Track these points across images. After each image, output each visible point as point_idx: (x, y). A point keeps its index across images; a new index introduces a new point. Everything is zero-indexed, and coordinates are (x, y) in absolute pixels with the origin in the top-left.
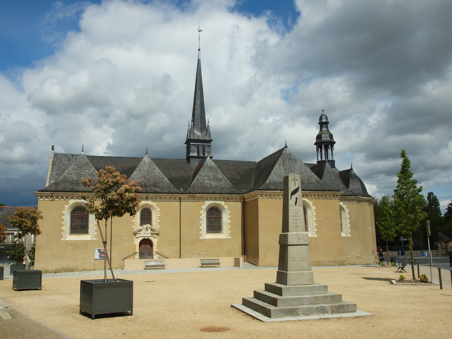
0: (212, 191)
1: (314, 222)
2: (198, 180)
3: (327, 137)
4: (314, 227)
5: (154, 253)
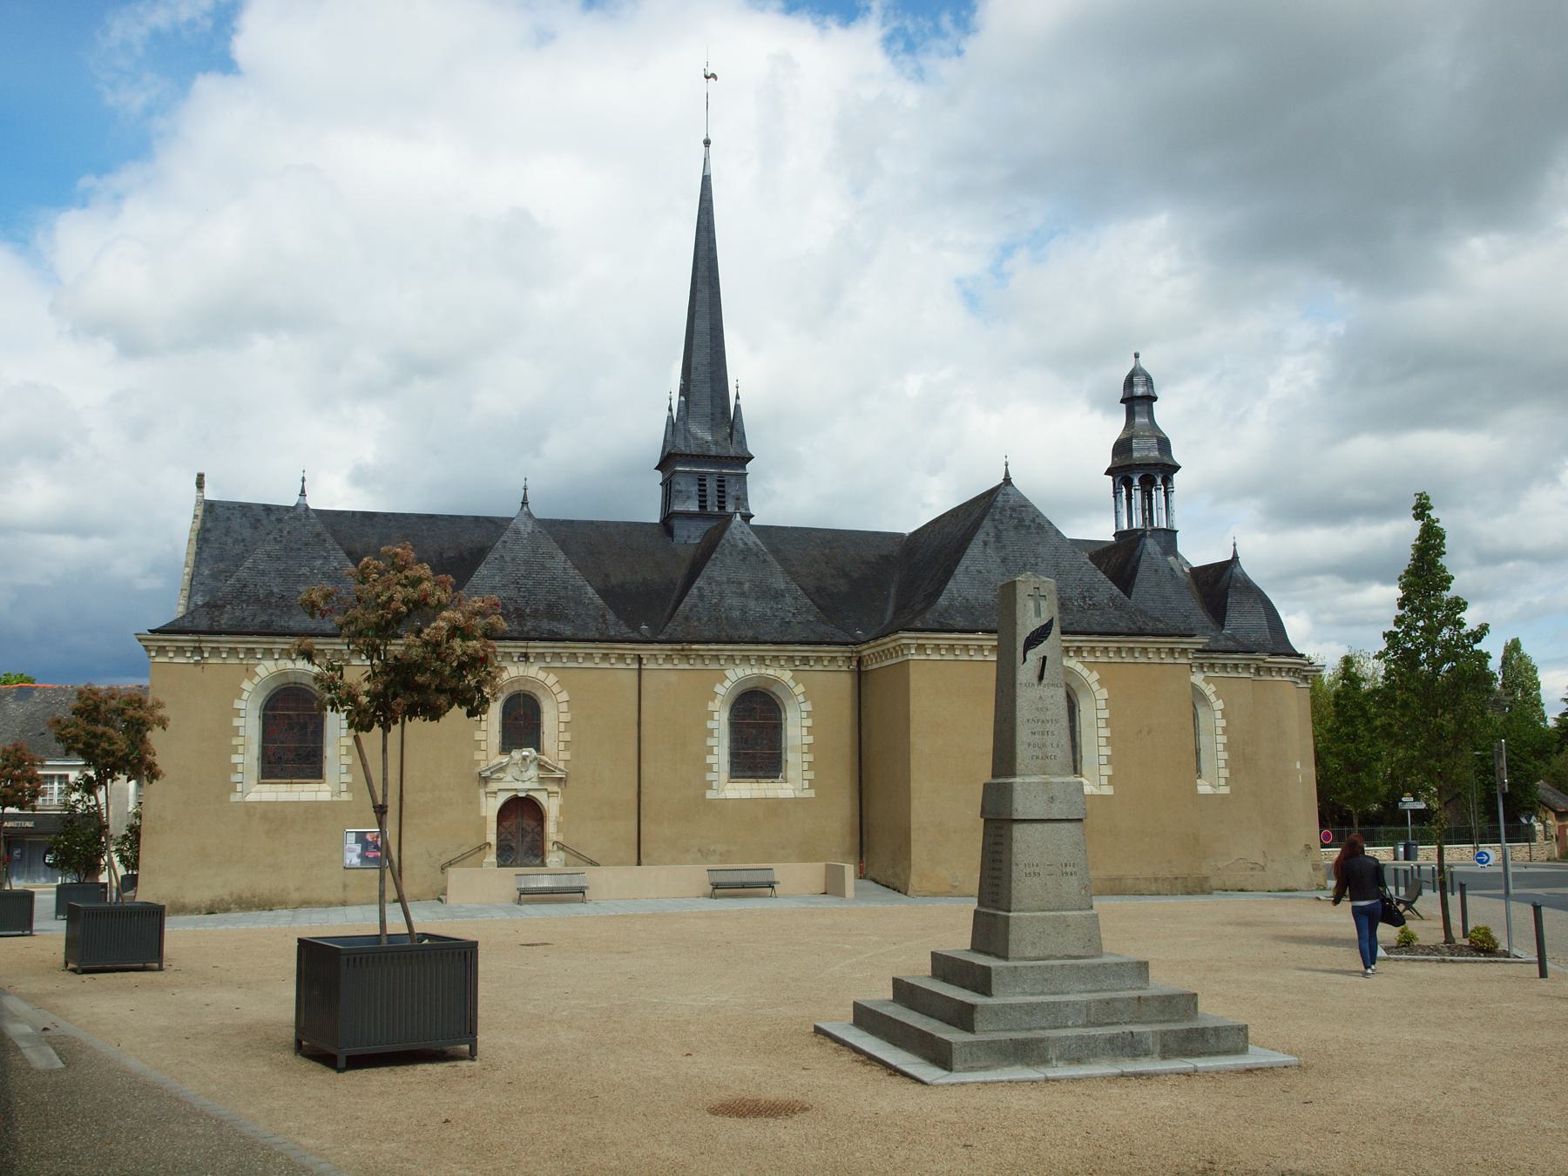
0: (750, 633)
1: (1103, 742)
2: (701, 597)
4: (1104, 760)
5: (549, 846)
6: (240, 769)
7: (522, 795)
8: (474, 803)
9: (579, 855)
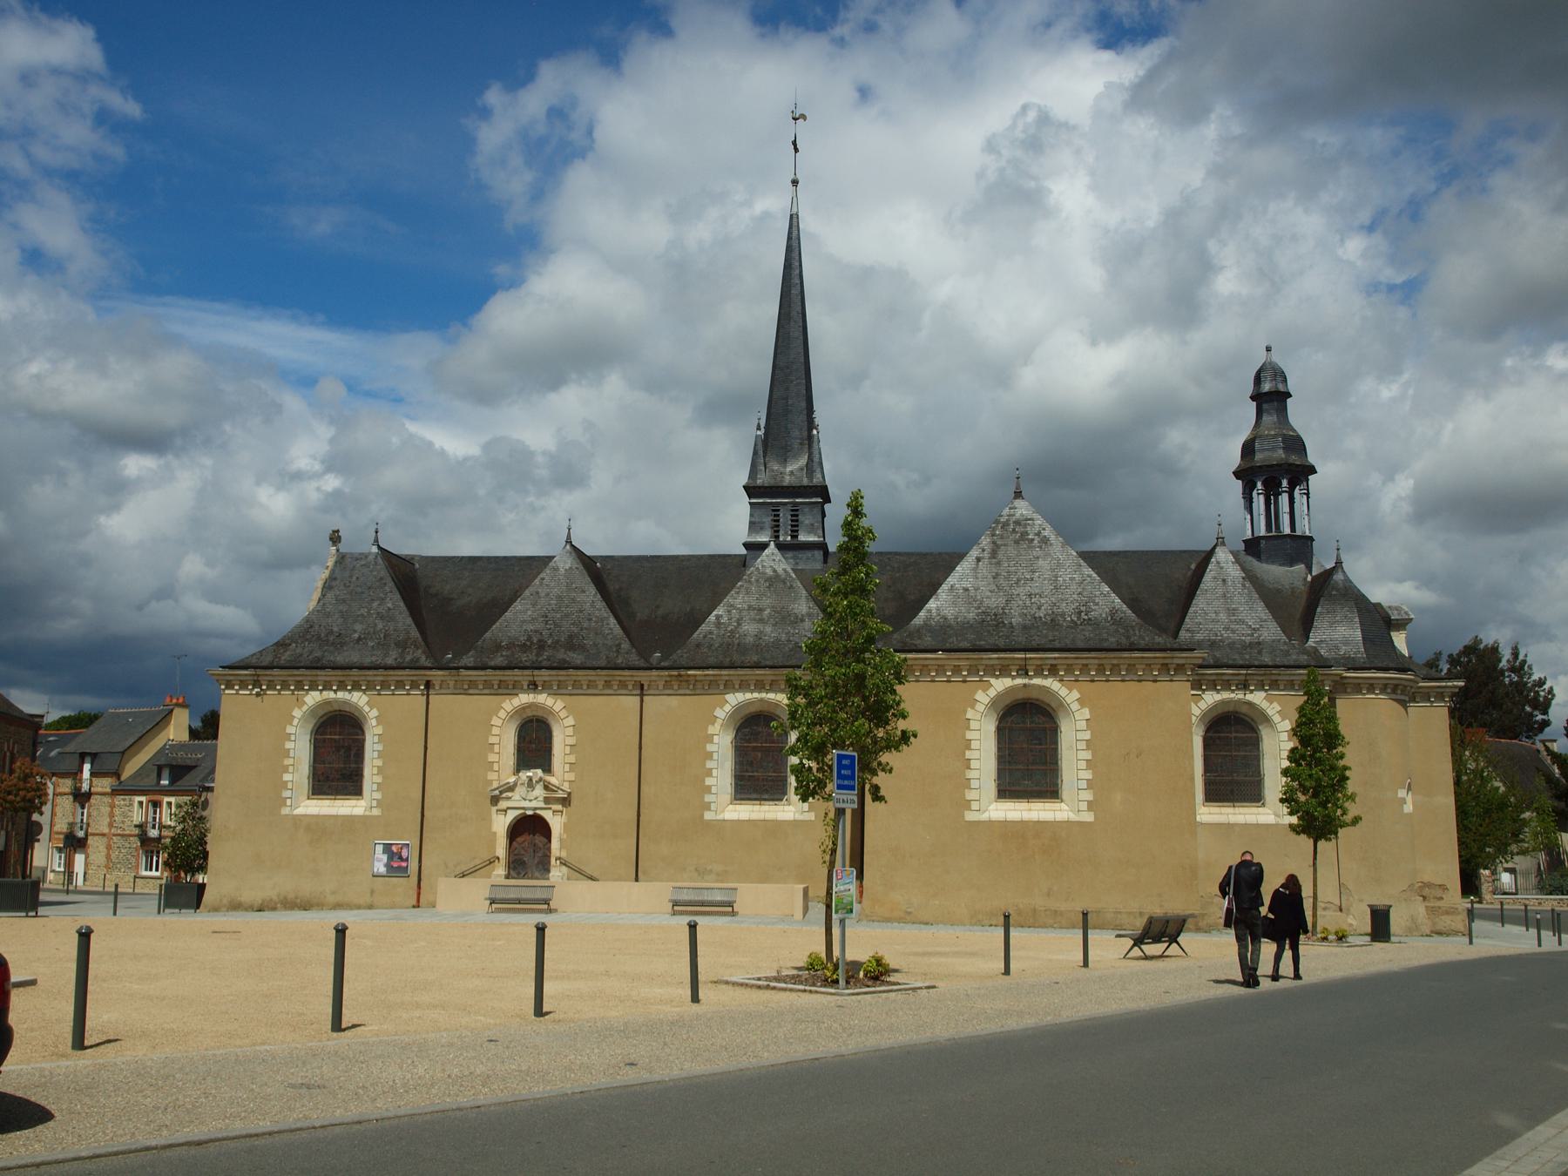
0: (755, 658)
1: (1083, 765)
2: (718, 624)
3: (1273, 449)
4: (1083, 784)
5: (553, 860)
7: (530, 813)
8: (488, 821)
9: (580, 872)
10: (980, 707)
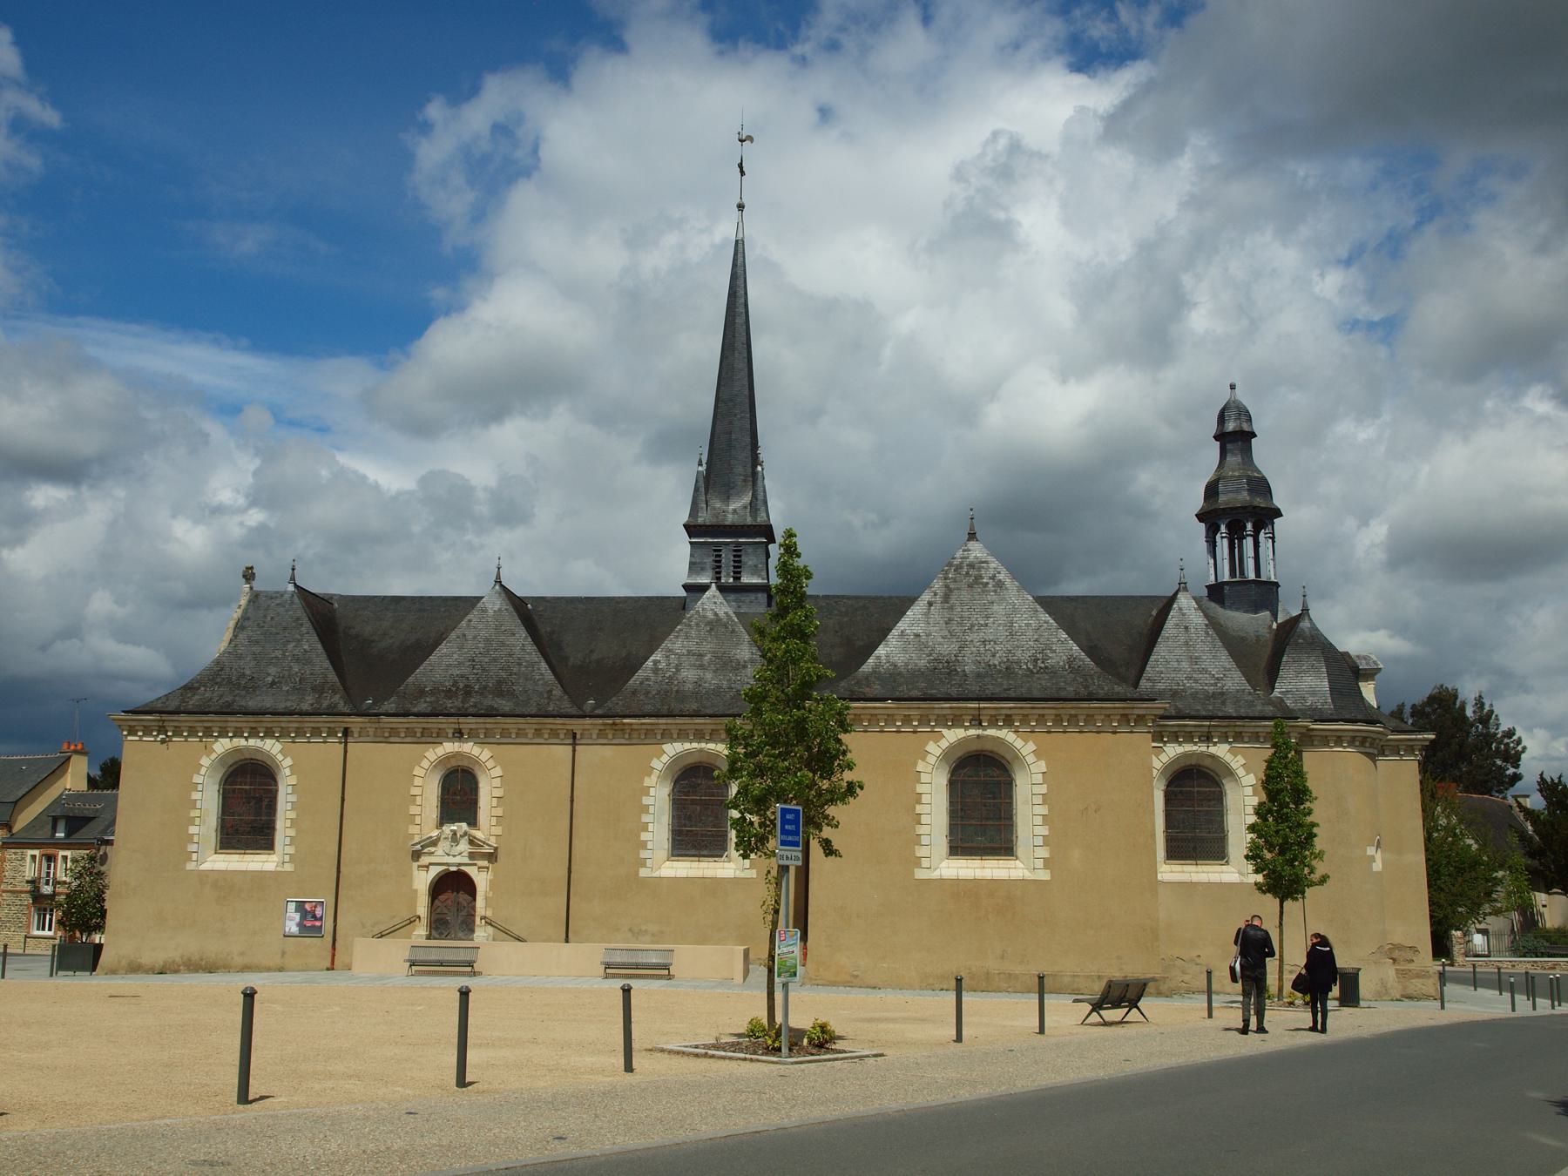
0: (694, 707)
1: (1039, 820)
2: (656, 670)
3: (1238, 491)
6: (650, 845)
7: (453, 869)
10: (931, 759)
